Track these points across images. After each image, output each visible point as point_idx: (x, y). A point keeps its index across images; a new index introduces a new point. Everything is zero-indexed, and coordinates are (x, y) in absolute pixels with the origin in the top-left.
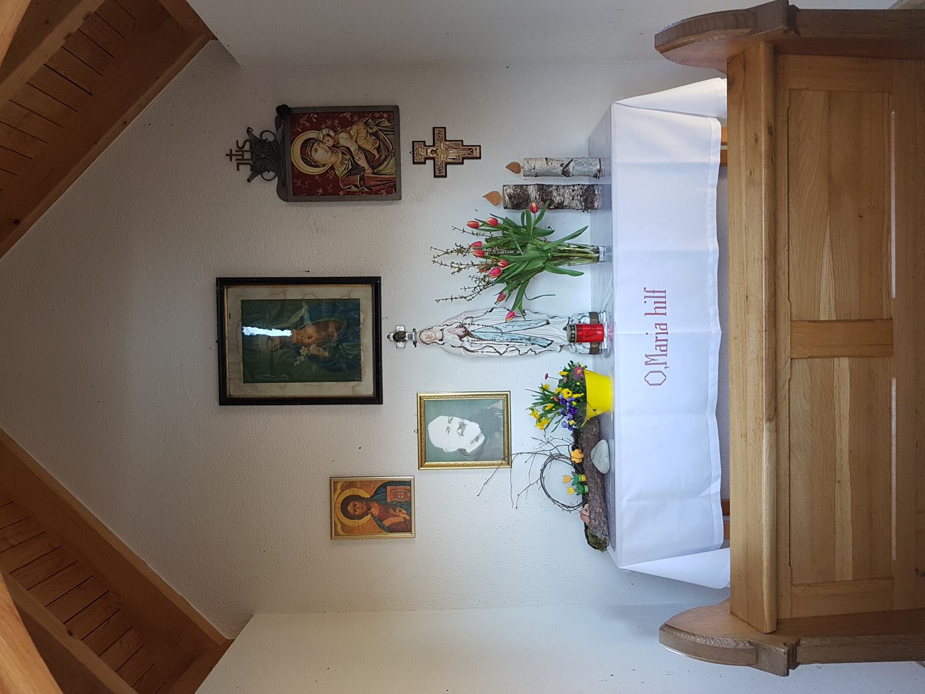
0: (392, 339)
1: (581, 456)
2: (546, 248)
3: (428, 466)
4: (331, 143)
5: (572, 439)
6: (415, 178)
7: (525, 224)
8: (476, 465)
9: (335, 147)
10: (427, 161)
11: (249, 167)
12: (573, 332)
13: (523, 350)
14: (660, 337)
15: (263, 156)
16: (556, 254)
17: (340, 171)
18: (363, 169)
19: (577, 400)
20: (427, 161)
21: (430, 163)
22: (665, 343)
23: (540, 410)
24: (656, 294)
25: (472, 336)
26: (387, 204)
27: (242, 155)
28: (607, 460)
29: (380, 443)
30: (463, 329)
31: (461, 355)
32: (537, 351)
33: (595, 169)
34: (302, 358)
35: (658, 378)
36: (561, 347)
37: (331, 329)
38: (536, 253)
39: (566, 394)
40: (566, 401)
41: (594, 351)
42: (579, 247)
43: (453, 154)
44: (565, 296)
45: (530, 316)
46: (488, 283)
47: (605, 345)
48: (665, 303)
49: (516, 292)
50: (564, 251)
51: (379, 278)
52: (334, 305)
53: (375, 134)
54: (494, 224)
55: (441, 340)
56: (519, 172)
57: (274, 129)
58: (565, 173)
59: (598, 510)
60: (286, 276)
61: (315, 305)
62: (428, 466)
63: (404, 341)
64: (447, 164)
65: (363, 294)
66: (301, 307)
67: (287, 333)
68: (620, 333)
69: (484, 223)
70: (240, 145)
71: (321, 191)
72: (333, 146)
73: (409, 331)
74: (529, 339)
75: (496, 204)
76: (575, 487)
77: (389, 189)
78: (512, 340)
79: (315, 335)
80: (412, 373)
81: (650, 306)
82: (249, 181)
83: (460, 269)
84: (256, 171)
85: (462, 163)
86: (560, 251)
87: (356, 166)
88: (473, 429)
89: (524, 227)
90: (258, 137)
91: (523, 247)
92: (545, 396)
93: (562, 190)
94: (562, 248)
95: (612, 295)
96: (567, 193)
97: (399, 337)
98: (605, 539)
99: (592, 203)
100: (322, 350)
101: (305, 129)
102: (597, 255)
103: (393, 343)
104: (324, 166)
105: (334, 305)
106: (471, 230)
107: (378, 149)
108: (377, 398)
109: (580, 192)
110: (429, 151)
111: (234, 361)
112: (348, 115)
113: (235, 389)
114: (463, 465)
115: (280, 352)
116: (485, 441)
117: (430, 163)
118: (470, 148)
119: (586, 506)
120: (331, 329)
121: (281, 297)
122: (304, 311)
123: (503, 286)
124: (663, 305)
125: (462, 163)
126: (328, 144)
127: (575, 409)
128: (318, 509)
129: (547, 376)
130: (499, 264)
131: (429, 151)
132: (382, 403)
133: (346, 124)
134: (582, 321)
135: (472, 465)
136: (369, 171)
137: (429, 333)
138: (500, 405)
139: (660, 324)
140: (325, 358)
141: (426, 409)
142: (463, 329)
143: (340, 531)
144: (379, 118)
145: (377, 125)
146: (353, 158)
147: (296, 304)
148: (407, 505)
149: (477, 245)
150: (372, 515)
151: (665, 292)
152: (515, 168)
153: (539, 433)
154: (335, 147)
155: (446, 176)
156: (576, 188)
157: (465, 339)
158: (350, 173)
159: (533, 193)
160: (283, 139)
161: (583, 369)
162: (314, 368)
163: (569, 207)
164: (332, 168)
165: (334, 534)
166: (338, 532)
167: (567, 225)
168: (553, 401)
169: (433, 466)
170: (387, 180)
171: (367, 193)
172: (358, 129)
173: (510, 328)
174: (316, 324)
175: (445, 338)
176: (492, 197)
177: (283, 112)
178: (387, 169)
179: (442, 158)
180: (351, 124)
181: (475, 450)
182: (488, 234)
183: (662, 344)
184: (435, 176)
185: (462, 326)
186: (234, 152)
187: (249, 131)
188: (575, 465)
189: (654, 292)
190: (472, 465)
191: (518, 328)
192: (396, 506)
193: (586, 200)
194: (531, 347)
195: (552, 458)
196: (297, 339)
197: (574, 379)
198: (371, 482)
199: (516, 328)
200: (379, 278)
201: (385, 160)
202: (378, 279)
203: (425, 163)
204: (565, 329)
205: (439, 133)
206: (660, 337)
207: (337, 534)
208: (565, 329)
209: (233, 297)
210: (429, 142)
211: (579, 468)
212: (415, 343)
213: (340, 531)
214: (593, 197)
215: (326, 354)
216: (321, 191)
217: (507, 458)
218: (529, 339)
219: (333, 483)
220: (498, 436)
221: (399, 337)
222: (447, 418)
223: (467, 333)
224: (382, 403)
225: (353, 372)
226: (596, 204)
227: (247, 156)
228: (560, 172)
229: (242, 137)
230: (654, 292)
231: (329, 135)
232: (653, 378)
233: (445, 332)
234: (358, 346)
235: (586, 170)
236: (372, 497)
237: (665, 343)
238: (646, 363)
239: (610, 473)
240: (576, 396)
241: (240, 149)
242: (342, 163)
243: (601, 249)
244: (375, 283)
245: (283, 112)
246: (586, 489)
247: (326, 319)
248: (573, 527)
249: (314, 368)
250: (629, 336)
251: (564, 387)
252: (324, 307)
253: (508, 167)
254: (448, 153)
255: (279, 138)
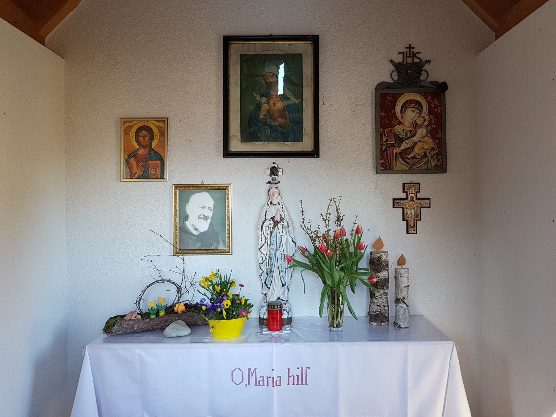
0: (273, 165)
1: (180, 311)
2: (341, 287)
3: (175, 192)
4: (419, 122)
5: (194, 303)
6: (393, 185)
7: (359, 271)
8: (176, 228)
9: (416, 125)
10: (405, 194)
11: (401, 61)
12: (276, 307)
13: (263, 266)
14: (270, 380)
15: (409, 71)
16: (336, 294)
17: (398, 129)
18: (399, 146)
19: (221, 312)
20: (405, 194)
21: (404, 196)
22: (266, 384)
23: (216, 280)
24: (304, 377)
25: (274, 227)
26: (373, 163)
27: (410, 57)
28: (174, 335)
29: (195, 156)
30: (279, 220)
31: (260, 218)
32: (262, 277)
33: (401, 324)
34: (258, 98)
35: (238, 379)
36: (265, 294)
37: (280, 120)
38: (337, 279)
39: (227, 303)
40: (221, 303)
41: (261, 321)
42: (341, 312)
43: (411, 213)
44: (305, 299)
45: (289, 271)
46: (314, 240)
47: (266, 331)
48: (298, 384)
49: (307, 262)
50: (338, 300)
51: (318, 157)
52: (298, 123)
53: (425, 155)
54: (359, 247)
55: (271, 203)
56: (398, 264)
57: (429, 80)
58: (398, 301)
59: (136, 326)
60: (320, 87)
61: (299, 109)
62: (175, 192)
63: (271, 175)
64: (403, 208)
65: (307, 145)
66: (297, 99)
67: (281, 91)
68: (275, 348)
69: (360, 238)
70: (417, 55)
71: (383, 114)
72: (417, 124)
73: (279, 179)
74: (271, 271)
75: (374, 246)
76: (155, 307)
77: (384, 165)
78: (270, 258)
79: (276, 108)
80: (246, 179)
81: (295, 372)
82: (391, 61)
83: (325, 220)
84: (398, 67)
85: (403, 220)
86: (338, 297)
87: (400, 141)
88: (204, 227)
89: (357, 269)
90: (424, 68)
91: (342, 269)
92: (226, 285)
93: (384, 297)
94: (341, 298)
95: (305, 341)
96: (382, 301)
97: (274, 171)
98: (112, 333)
99: (375, 321)
100: (265, 113)
101: (429, 103)
102: (335, 326)
103: (269, 167)
104: (402, 117)
105: (298, 123)
106: (355, 229)
107: (414, 158)
108: (228, 154)
109: (383, 311)
110: (413, 195)
111: (257, 48)
112: (439, 135)
113: (236, 49)
114: (176, 218)
115: (263, 82)
116: (194, 235)
117: (404, 196)
118: (415, 226)
119: (139, 317)
120: (280, 120)
121: (304, 84)
122: (294, 100)
123: (311, 250)
124: (296, 383)
125: (403, 220)
126: (418, 120)
127: (215, 310)
128: (144, 108)
129: (242, 286)
130: (329, 251)
131: (413, 195)
132: (224, 157)
133: (433, 134)
134: (285, 312)
135: (176, 225)
136: (398, 150)
137: (277, 194)
138: (221, 247)
139: (280, 380)
140: (259, 116)
141: (220, 191)
142: (279, 220)
143: (126, 125)
144: (437, 158)
145: (432, 157)
146: (408, 139)
147: (299, 95)
148: (145, 176)
149: (343, 232)
150: (138, 149)
151: (306, 384)
152: (401, 261)
153: (199, 278)
154: (416, 125)
155: (394, 207)
156: (386, 308)
157: (272, 222)
158: (397, 136)
159: (383, 275)
160: (421, 87)
161: (247, 317)
162: (251, 107)
163: (371, 302)
164: (400, 123)
165: (124, 121)
166: (126, 124)
167: (357, 301)
168: (222, 291)
169: (175, 195)
170: (391, 164)
171: (381, 149)
172: (429, 143)
173: (279, 256)
174: (284, 109)
175: (272, 206)
176: (379, 243)
177: (443, 87)
178: (399, 164)
179: (408, 205)
180: (433, 137)
181: (187, 228)
182: (352, 242)
183: (265, 382)
184: (394, 199)
185: (282, 219)
186: (412, 50)
187: (428, 61)
188: (173, 306)
189: (306, 375)
190: (176, 225)
191: (280, 263)
192: (145, 167)
193: (377, 315)
194: (265, 272)
195: (179, 289)
196: (273, 95)
197: (239, 308)
198: (164, 148)
199: (280, 261)
200: (318, 157)
201: (406, 162)
202: (225, 37)
203: (404, 192)
204: (279, 298)
205: (426, 202)
206: (270, 380)
207: (124, 122)
208: (279, 298)
209: (305, 48)
210: (419, 195)
211: (170, 310)
212: (269, 183)
213: (126, 125)
214: (381, 322)
215: (261, 117)
216: (383, 114)
217: (180, 252)
218: (271, 271)
219: (164, 120)
220: (198, 245)
221: (274, 171)
222: (212, 206)
223: (276, 223)
224: (224, 157)
225: (248, 135)
226: (374, 323)
227: (410, 60)
228: (398, 297)
229: (424, 57)
230: (306, 375)
231: (425, 121)
232: (237, 374)
233: (277, 206)
234: (268, 140)
235: (401, 317)
236: (153, 149)
237: (266, 384)
238: (249, 369)
239: (165, 339)
240: (224, 312)
241: (415, 55)
242: (404, 130)
243: (340, 329)
244: (315, 153)
245: (443, 87)
246: (153, 317)
247: (288, 117)
248: (125, 305)
249: (251, 107)
250: (272, 355)
251: (233, 301)
252: (297, 115)
253: (402, 257)
254: (410, 210)
255: (422, 84)
